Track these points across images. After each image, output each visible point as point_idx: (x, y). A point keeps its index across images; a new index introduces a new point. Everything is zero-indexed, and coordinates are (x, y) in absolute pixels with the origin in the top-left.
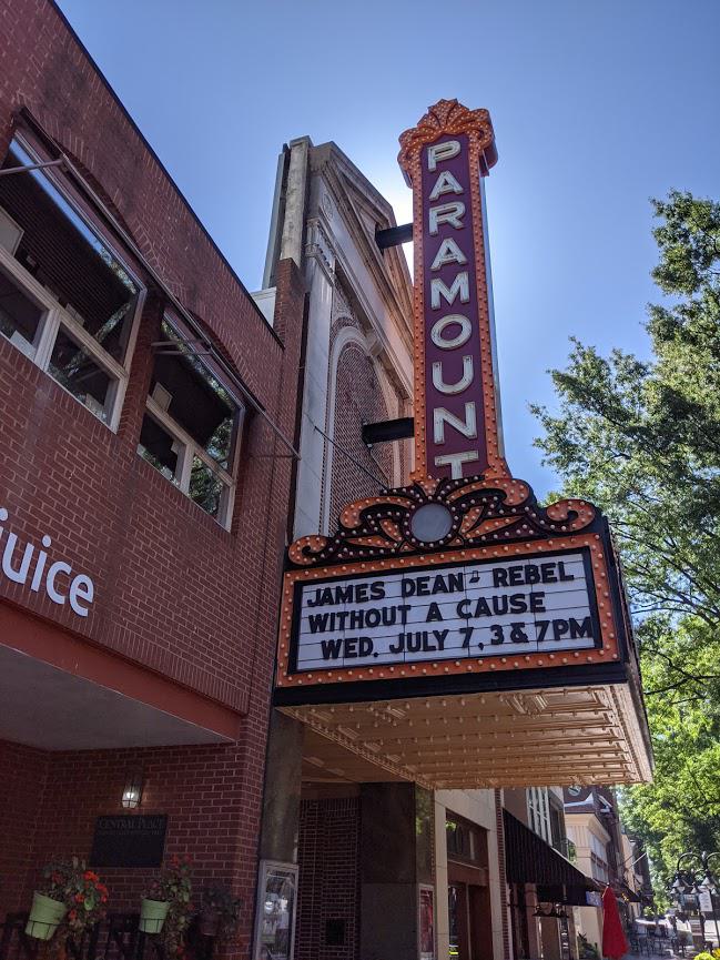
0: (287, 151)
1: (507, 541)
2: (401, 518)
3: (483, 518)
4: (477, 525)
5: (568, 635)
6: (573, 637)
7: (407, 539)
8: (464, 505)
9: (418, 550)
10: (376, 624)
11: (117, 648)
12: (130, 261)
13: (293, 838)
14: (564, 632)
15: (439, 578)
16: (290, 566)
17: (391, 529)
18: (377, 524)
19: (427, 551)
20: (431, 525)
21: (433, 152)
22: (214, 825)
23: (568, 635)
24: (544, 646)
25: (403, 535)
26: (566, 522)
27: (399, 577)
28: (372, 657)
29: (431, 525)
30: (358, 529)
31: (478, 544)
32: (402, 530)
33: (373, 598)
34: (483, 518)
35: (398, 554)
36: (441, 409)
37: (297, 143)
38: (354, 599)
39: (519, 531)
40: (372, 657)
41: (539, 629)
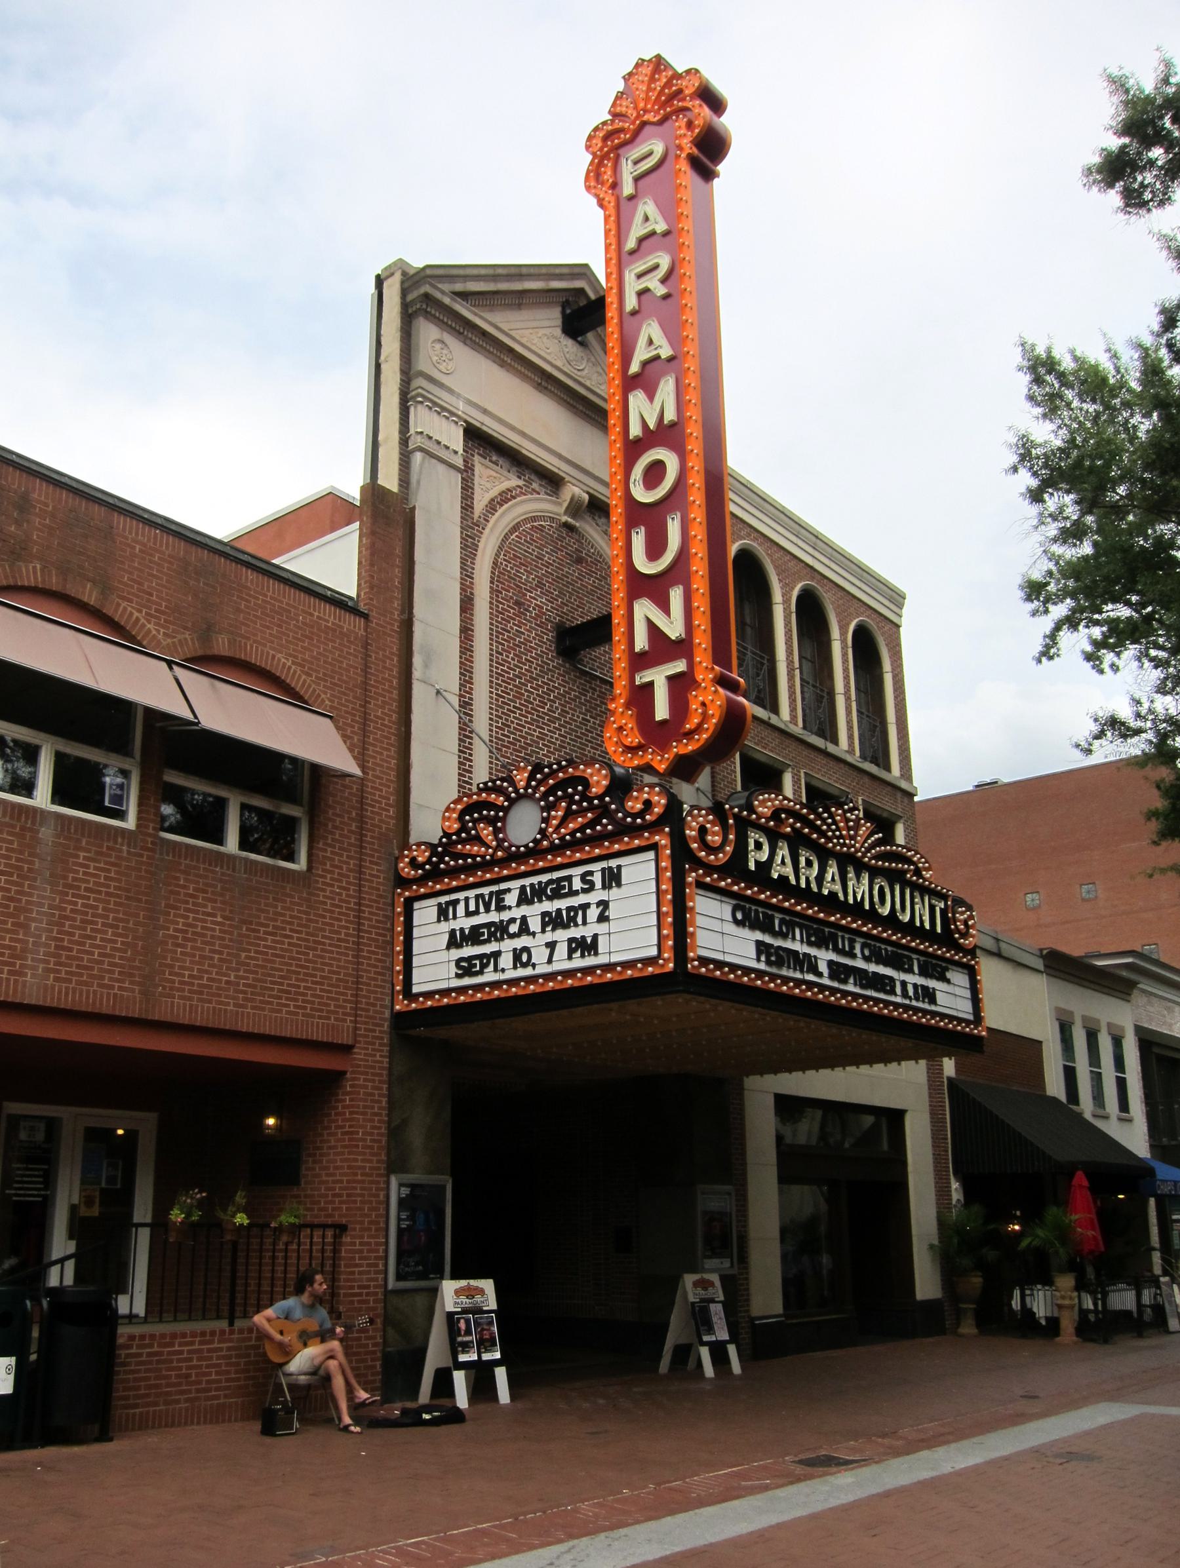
0: (379, 282)
1: (587, 840)
2: (497, 822)
3: (569, 815)
4: (563, 822)
5: (578, 954)
6: (583, 956)
7: (500, 842)
8: (551, 798)
9: (519, 857)
10: (502, 939)
11: (169, 1019)
12: (561, 280)
13: (38, 1263)
14: (575, 950)
15: (523, 888)
16: (403, 882)
17: (486, 832)
18: (475, 828)
19: (519, 857)
20: (524, 826)
21: (633, 276)
22: (340, 1202)
23: (578, 954)
24: (556, 967)
25: (496, 838)
26: (641, 814)
27: (433, 901)
28: (530, 968)
29: (524, 826)
30: (458, 833)
31: (564, 845)
32: (496, 831)
33: (585, 891)
34: (569, 815)
35: (495, 862)
36: (673, 636)
37: (389, 272)
38: (493, 907)
39: (598, 828)
40: (530, 968)
41: (548, 951)
